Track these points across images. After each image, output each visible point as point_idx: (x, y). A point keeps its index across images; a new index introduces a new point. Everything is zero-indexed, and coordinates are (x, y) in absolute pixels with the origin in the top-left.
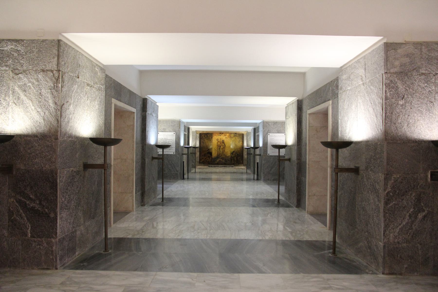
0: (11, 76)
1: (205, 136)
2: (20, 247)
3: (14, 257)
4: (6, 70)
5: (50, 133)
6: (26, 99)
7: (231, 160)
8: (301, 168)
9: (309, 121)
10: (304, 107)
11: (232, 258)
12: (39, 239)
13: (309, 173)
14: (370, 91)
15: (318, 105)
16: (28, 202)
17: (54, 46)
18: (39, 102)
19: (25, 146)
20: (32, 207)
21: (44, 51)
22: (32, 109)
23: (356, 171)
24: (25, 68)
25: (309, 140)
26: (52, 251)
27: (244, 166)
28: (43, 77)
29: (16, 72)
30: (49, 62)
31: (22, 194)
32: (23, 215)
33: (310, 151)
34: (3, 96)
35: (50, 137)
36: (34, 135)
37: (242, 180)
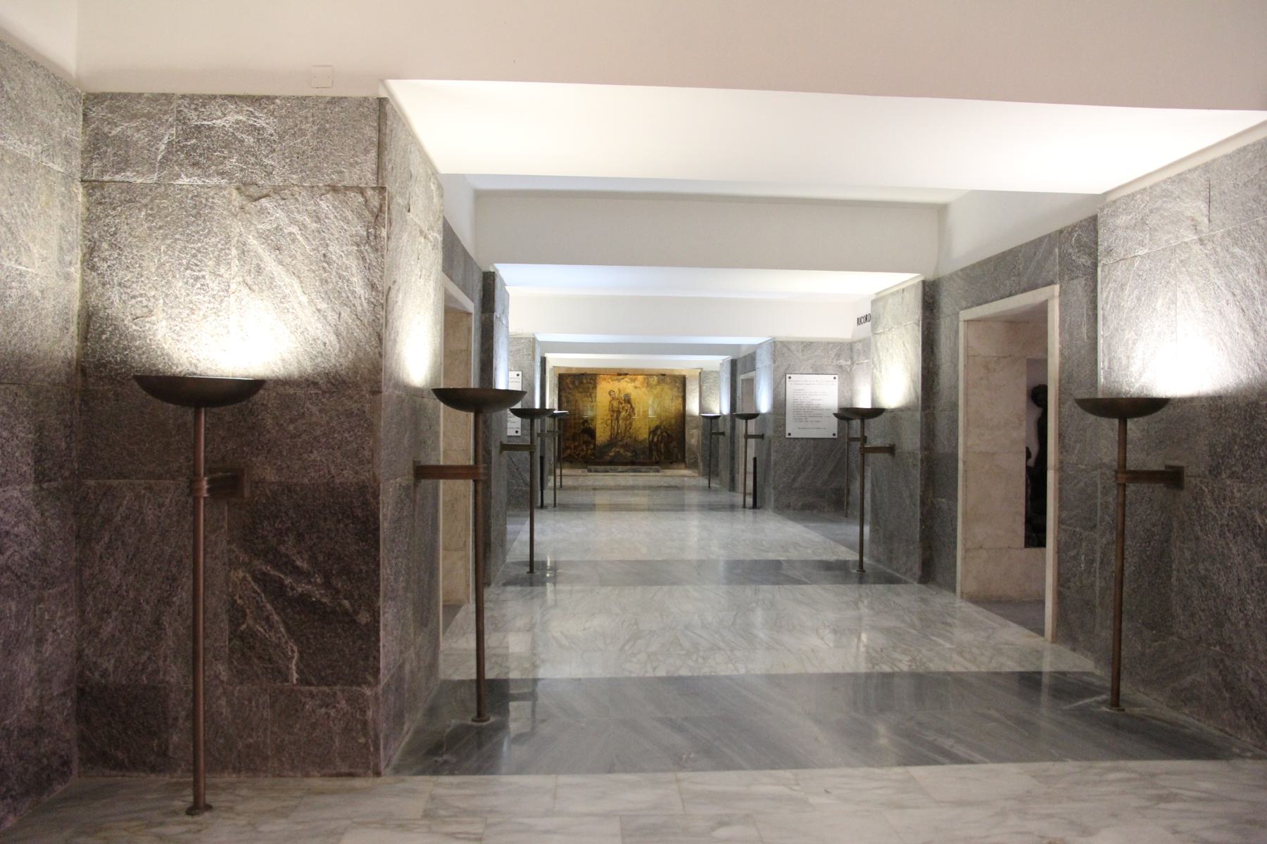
0: (236, 204)
1: (573, 383)
2: (267, 713)
3: (251, 741)
4: (221, 188)
5: (356, 373)
6: (283, 273)
7: (651, 450)
8: (937, 472)
9: (967, 341)
10: (946, 303)
11: (704, 725)
12: (326, 689)
13: (966, 486)
14: (1229, 260)
15: (1002, 298)
16: (288, 581)
17: (366, 117)
18: (321, 280)
19: (277, 413)
20: (302, 595)
21: (336, 132)
22: (299, 303)
23: (1173, 477)
24: (278, 180)
25: (966, 394)
26: (365, 723)
27: (687, 467)
28: (335, 208)
29: (251, 192)
30: (351, 165)
31: (270, 556)
32: (276, 617)
33: (967, 423)
34: (210, 263)
35: (357, 386)
36: (307, 380)
37: (732, 507)
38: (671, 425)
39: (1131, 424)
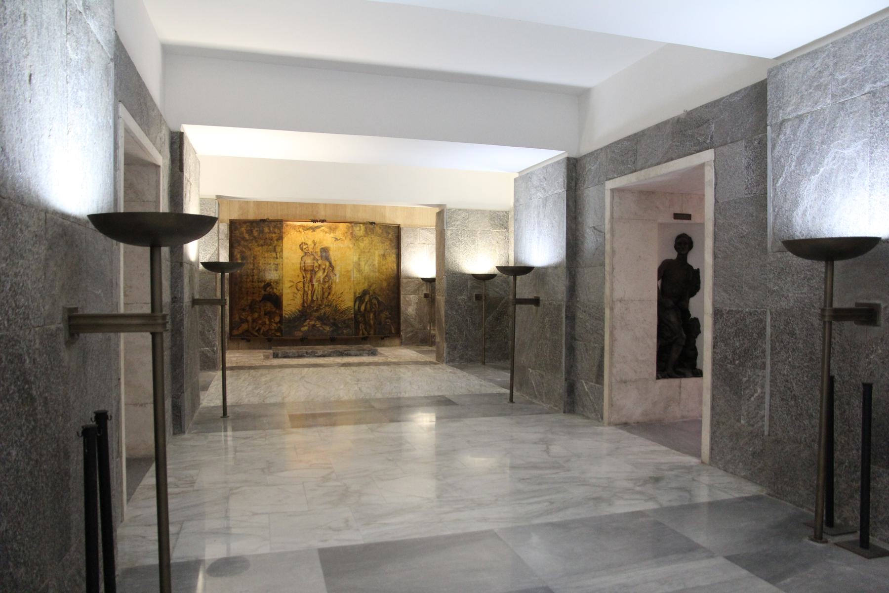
1: (250, 232)
38: (381, 289)
39: (518, 278)
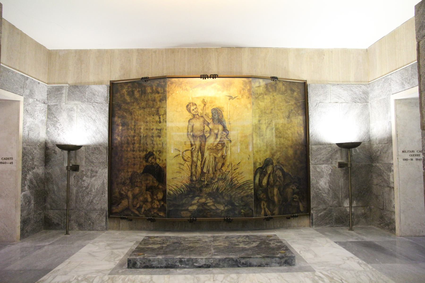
1: (131, 94)
